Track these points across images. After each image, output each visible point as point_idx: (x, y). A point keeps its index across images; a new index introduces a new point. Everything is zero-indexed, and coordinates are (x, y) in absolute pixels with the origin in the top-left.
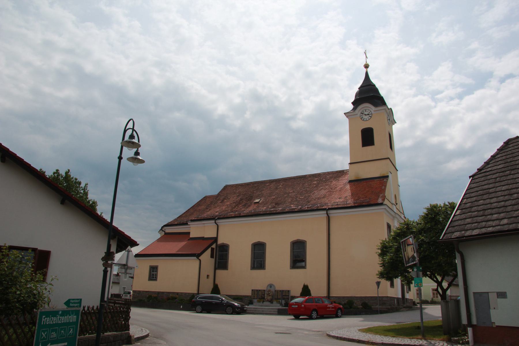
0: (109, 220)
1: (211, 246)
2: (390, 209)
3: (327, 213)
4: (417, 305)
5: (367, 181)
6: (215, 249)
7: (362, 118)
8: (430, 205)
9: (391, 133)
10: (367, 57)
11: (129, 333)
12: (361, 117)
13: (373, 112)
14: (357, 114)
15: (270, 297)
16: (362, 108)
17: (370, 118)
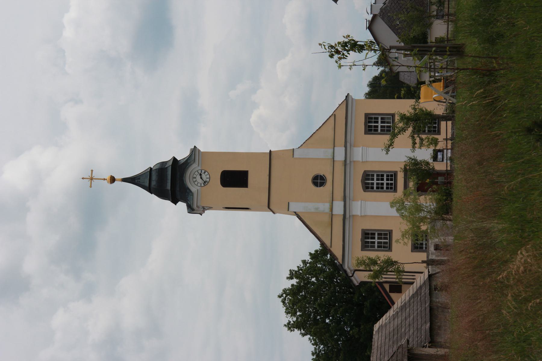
1: (387, 292)
6: (390, 284)
8: (288, 330)
9: (212, 209)
13: (199, 168)
14: (198, 190)
16: (189, 177)
17: (206, 173)
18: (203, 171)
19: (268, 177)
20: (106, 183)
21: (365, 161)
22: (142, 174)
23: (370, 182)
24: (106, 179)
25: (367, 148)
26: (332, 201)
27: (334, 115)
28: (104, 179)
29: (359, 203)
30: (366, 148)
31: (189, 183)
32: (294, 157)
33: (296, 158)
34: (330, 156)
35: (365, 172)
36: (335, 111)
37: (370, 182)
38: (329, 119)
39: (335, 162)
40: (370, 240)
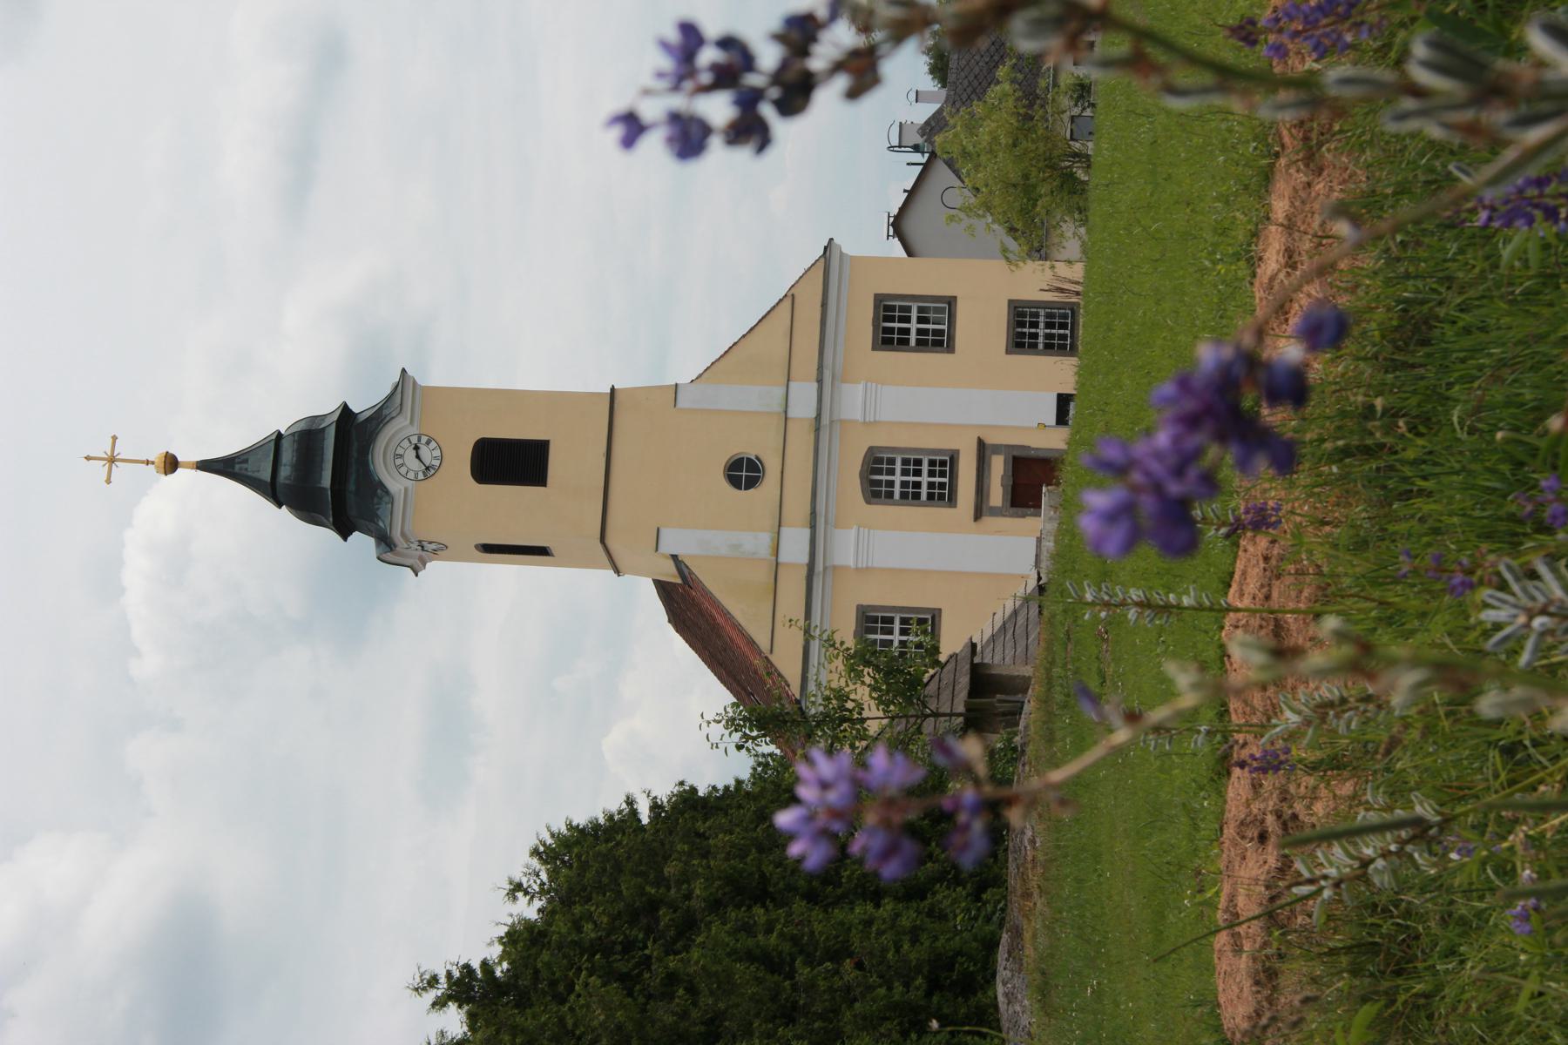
0: (921, 167)
2: (820, 452)
4: (1549, 744)
5: (821, 569)
10: (112, 479)
13: (414, 430)
14: (406, 489)
17: (433, 444)
18: (424, 439)
19: (604, 459)
23: (884, 478)
24: (153, 463)
25: (879, 386)
26: (780, 526)
27: (790, 297)
28: (148, 462)
32: (680, 404)
33: (681, 409)
34: (777, 406)
35: (871, 449)
36: (793, 286)
37: (884, 478)
38: (776, 310)
39: (788, 422)
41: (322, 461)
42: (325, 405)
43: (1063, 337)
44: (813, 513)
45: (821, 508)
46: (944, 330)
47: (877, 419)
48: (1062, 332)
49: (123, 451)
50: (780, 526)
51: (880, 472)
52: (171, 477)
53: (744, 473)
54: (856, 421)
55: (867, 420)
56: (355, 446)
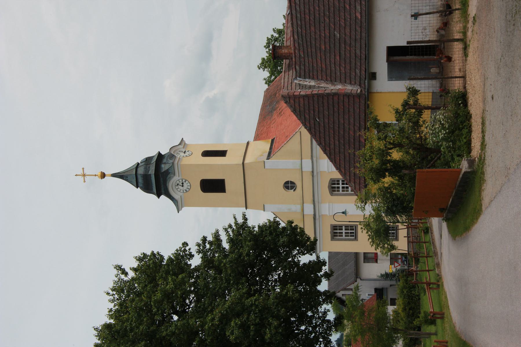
3: (372, 258)
5: (318, 218)
7: (186, 190)
11: (388, 305)
12: (185, 191)
15: (143, 255)
16: (172, 188)
17: (187, 182)
18: (184, 180)
19: (243, 184)
20: (98, 179)
21: (331, 171)
22: (130, 169)
23: (336, 186)
24: (97, 175)
26: (303, 203)
28: (95, 175)
29: (327, 205)
30: (332, 204)
31: (172, 190)
32: (266, 168)
33: (267, 169)
34: (298, 166)
37: (336, 186)
39: (303, 172)
40: (338, 231)
41: (152, 184)
42: (153, 153)
43: (393, 233)
44: (314, 201)
45: (316, 200)
46: (354, 232)
47: (333, 171)
48: (393, 232)
49: (87, 172)
50: (303, 203)
51: (334, 184)
52: (103, 179)
53: (289, 185)
54: (325, 172)
55: (329, 171)
56: (162, 179)
